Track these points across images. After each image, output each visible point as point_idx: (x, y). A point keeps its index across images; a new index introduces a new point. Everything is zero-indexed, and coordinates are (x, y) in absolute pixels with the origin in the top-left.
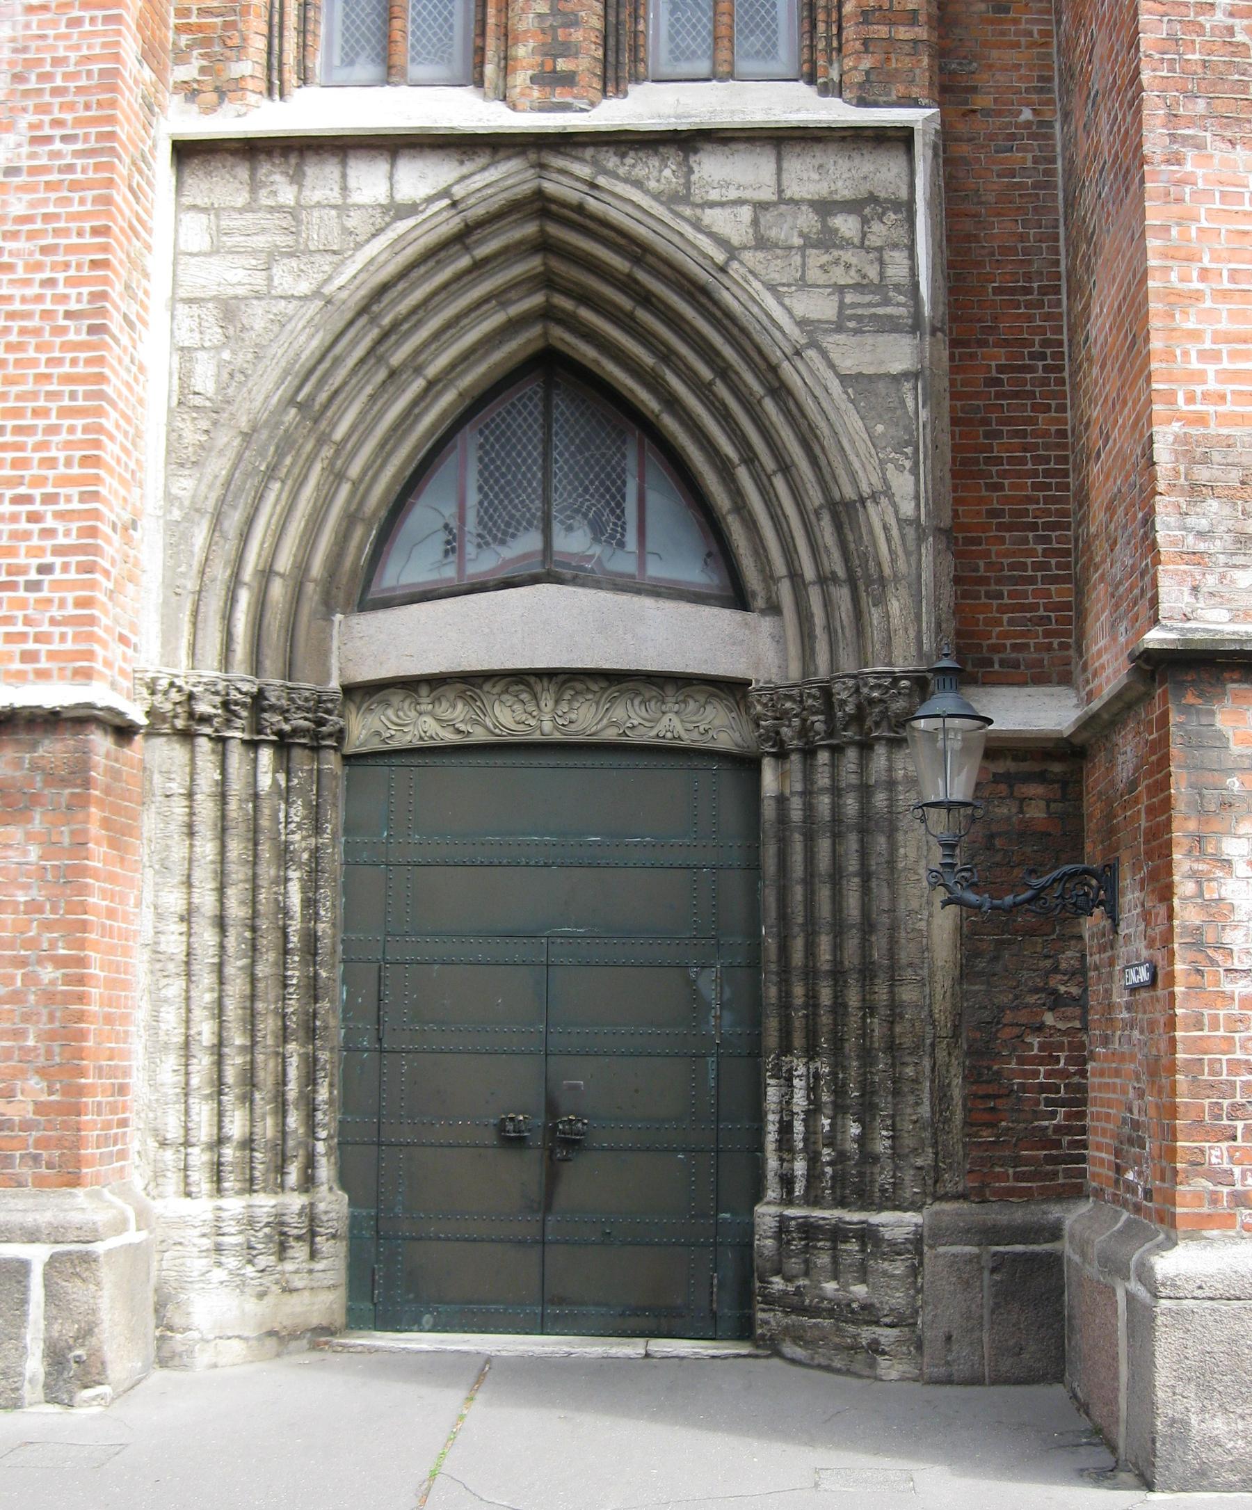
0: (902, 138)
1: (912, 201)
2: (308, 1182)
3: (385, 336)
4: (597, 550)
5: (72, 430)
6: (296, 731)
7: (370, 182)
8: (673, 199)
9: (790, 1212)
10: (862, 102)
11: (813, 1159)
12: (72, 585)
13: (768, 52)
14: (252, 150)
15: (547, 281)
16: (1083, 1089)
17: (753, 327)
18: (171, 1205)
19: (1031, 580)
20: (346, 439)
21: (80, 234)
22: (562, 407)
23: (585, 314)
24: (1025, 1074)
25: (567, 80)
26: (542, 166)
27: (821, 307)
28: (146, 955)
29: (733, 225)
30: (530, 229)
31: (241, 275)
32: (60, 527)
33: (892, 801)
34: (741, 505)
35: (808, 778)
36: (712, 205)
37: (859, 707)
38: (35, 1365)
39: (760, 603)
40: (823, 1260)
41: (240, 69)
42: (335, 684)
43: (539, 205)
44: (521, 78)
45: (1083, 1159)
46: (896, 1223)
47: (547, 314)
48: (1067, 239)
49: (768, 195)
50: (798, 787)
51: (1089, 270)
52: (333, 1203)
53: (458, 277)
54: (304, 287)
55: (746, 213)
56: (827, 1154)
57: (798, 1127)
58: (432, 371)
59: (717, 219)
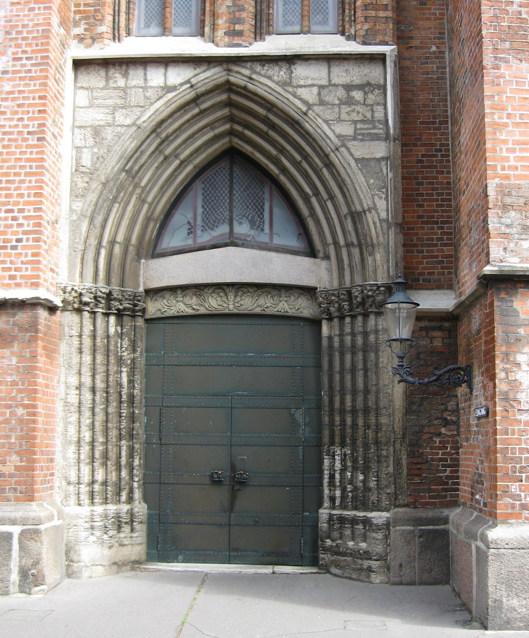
0: (381, 58)
1: (385, 85)
2: (130, 499)
3: (163, 142)
4: (252, 232)
5: (30, 181)
6: (125, 309)
7: (156, 77)
8: (284, 84)
9: (334, 512)
10: (364, 43)
11: (344, 490)
12: (30, 247)
13: (325, 22)
14: (106, 63)
15: (231, 119)
16: (457, 460)
17: (318, 138)
18: (72, 509)
19: (436, 245)
20: (146, 186)
21: (34, 99)
22: (237, 172)
23: (247, 133)
24: (433, 454)
25: (240, 34)
26: (229, 70)
27: (347, 130)
28: (62, 403)
29: (310, 95)
30: (224, 97)
31: (102, 116)
32: (25, 222)
33: (377, 338)
34: (313, 214)
35: (341, 329)
36: (301, 86)
37: (363, 299)
38: (15, 577)
39: (321, 255)
40: (348, 532)
41: (101, 29)
42: (141, 289)
43: (228, 87)
44: (220, 33)
45: (457, 490)
46: (379, 517)
47: (231, 133)
48: (451, 101)
49: (324, 82)
50: (337, 332)
51: (460, 114)
52: (141, 508)
53: (193, 117)
54: (128, 121)
55: (315, 90)
56: (349, 488)
57: (337, 476)
58: (182, 157)
59: (303, 93)
